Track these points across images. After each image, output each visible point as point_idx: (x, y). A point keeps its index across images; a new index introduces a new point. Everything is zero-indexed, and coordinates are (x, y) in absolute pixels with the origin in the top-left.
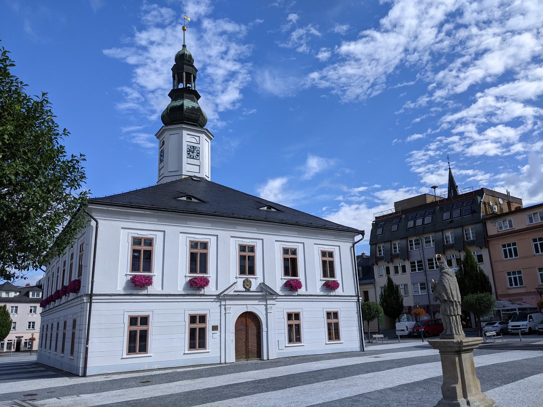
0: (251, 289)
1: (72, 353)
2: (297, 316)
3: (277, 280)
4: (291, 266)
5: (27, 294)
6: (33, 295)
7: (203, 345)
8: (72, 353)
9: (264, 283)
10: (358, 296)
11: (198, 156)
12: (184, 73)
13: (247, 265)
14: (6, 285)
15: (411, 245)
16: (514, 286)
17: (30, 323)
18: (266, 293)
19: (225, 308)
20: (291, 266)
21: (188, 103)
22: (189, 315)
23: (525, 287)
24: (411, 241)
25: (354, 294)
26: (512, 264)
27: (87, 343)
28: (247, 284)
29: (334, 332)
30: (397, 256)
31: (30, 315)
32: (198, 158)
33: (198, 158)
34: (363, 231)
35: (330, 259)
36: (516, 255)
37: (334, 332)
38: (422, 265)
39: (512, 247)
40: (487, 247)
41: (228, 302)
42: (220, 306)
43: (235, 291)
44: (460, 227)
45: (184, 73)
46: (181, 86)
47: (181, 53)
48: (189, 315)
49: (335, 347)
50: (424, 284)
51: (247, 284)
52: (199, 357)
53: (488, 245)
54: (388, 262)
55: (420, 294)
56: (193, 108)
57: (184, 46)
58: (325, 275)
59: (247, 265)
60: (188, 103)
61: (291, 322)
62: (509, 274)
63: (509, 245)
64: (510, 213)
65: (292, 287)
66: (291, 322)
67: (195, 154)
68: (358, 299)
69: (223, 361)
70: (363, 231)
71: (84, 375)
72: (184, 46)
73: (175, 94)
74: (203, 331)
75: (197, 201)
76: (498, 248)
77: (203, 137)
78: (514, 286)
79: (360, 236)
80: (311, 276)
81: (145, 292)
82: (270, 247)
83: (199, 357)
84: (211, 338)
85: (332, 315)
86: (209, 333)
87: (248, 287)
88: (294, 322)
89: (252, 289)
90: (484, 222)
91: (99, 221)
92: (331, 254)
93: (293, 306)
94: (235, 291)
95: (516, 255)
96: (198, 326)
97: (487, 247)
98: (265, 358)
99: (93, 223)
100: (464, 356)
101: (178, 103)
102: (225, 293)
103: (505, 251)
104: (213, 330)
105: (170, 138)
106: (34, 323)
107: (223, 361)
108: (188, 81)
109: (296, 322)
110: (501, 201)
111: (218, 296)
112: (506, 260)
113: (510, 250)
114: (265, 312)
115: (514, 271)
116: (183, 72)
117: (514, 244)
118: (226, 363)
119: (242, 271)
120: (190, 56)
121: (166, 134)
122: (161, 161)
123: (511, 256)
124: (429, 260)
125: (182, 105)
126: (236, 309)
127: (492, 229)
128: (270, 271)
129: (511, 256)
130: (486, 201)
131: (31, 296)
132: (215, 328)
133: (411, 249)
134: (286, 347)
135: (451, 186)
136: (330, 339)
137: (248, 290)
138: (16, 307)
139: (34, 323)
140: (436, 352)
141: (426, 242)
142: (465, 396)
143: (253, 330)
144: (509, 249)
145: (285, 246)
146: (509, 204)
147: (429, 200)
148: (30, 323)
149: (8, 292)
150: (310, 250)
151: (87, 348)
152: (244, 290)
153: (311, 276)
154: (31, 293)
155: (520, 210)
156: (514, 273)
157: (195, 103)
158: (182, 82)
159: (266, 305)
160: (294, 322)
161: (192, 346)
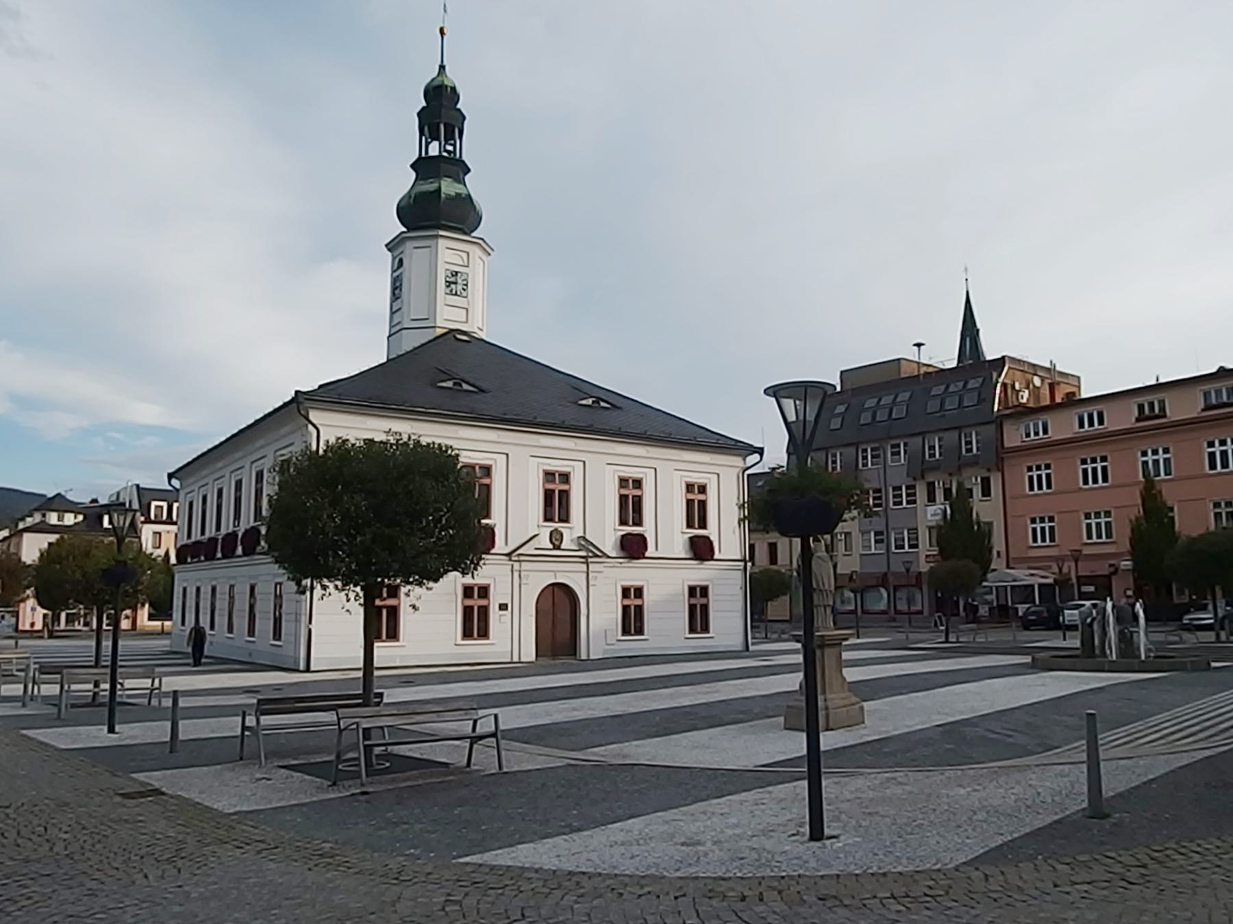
0: (563, 547)
1: (277, 634)
3: (608, 535)
4: (631, 508)
7: (484, 634)
8: (277, 634)
9: (584, 538)
10: (744, 560)
13: (556, 503)
14: (56, 500)
15: (865, 458)
16: (1095, 539)
18: (589, 552)
20: (631, 508)
21: (448, 187)
24: (865, 451)
25: (739, 557)
27: (310, 622)
28: (556, 539)
29: (699, 618)
33: (464, 294)
34: (762, 449)
35: (702, 497)
37: (699, 618)
38: (880, 498)
41: (525, 566)
46: (434, 149)
47: (436, 83)
49: (700, 643)
50: (881, 533)
51: (556, 539)
52: (477, 650)
54: (915, 479)
55: (873, 551)
56: (458, 195)
57: (442, 67)
58: (690, 525)
59: (556, 503)
60: (448, 187)
64: (1053, 407)
65: (633, 547)
67: (460, 287)
70: (762, 449)
71: (308, 670)
72: (442, 67)
73: (423, 166)
74: (484, 611)
77: (476, 252)
78: (1104, 539)
79: (756, 457)
80: (667, 529)
82: (597, 469)
83: (477, 650)
85: (698, 592)
90: (999, 422)
92: (703, 489)
93: (633, 573)
96: (476, 602)
98: (584, 657)
100: (827, 651)
101: (429, 187)
102: (519, 552)
105: (415, 255)
108: (449, 137)
110: (1037, 382)
111: (509, 555)
113: (1095, 470)
119: (548, 518)
120: (454, 89)
121: (409, 245)
122: (395, 296)
124: (894, 489)
125: (439, 189)
126: (538, 578)
127: (1014, 436)
128: (596, 517)
129: (1095, 481)
130: (1008, 381)
131: (106, 524)
132: (503, 607)
133: (865, 465)
136: (692, 630)
140: (799, 646)
141: (893, 454)
142: (824, 692)
145: (689, 480)
146: (1052, 387)
147: (906, 371)
149: (62, 511)
150: (667, 476)
151: (310, 631)
153: (667, 529)
155: (1072, 401)
157: (461, 186)
158: (438, 139)
161: (467, 634)
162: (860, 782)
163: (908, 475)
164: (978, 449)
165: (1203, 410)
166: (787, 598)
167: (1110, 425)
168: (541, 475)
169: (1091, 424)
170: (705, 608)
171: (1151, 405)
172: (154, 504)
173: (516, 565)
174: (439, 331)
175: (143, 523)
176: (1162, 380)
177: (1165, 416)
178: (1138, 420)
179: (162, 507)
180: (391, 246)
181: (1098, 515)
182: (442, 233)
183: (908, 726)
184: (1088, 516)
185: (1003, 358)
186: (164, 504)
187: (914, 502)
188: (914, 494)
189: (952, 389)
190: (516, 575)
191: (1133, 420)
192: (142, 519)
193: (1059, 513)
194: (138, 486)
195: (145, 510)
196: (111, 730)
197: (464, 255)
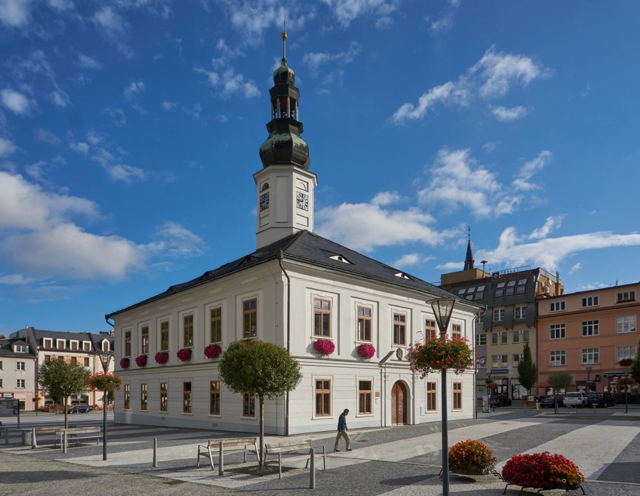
2: (327, 384)
5: (10, 348)
6: (18, 349)
11: (306, 206)
12: (289, 99)
17: (18, 381)
19: (385, 376)
22: (316, 380)
23: (567, 366)
26: (559, 343)
30: (499, 324)
31: (18, 372)
32: (306, 209)
36: (563, 336)
39: (560, 329)
40: (536, 326)
42: (381, 373)
43: (391, 360)
44: (512, 305)
45: (289, 99)
48: (316, 380)
53: (537, 325)
54: (486, 331)
61: (320, 391)
62: (553, 353)
63: (558, 326)
66: (320, 391)
67: (304, 204)
68: (476, 372)
69: (383, 425)
71: (286, 435)
75: (346, 262)
76: (545, 329)
80: (346, 338)
81: (327, 357)
84: (375, 404)
86: (374, 399)
87: (400, 357)
88: (323, 391)
89: (403, 359)
91: (290, 279)
94: (391, 360)
95: (563, 336)
97: (536, 326)
99: (284, 279)
103: (553, 332)
104: (376, 396)
106: (23, 381)
107: (383, 425)
109: (326, 391)
112: (552, 341)
113: (558, 331)
114: (411, 381)
115: (557, 350)
116: (287, 97)
117: (563, 326)
118: (385, 426)
123: (558, 336)
125: (291, 141)
129: (558, 336)
131: (15, 351)
132: (377, 394)
134: (425, 413)
135: (468, 261)
137: (400, 359)
138: (23, 363)
139: (23, 381)
143: (401, 395)
144: (557, 330)
148: (18, 381)
152: (397, 359)
153: (346, 338)
154: (15, 347)
156: (558, 353)
159: (413, 375)
160: (323, 391)
162: (63, 481)
163: (483, 330)
164: (501, 319)
165: (617, 303)
166: (519, 384)
167: (568, 309)
168: (393, 317)
169: (558, 309)
170: (327, 397)
171: (626, 294)
172: (45, 339)
173: (383, 369)
174: (295, 231)
175: (38, 350)
176: (619, 284)
177: (634, 300)
178: (618, 302)
179: (50, 341)
180: (256, 177)
181: (590, 350)
182: (295, 168)
183: (181, 457)
184: (584, 351)
185: (538, 269)
186: (51, 339)
187: (485, 343)
188: (485, 339)
189: (520, 283)
190: (383, 374)
191: (616, 303)
192: (38, 348)
193: (601, 347)
194: (33, 328)
195: (40, 342)
196: (105, 458)
197: (306, 184)
